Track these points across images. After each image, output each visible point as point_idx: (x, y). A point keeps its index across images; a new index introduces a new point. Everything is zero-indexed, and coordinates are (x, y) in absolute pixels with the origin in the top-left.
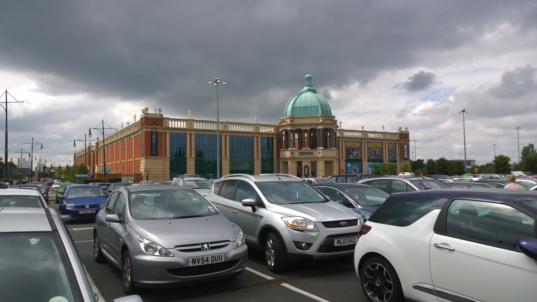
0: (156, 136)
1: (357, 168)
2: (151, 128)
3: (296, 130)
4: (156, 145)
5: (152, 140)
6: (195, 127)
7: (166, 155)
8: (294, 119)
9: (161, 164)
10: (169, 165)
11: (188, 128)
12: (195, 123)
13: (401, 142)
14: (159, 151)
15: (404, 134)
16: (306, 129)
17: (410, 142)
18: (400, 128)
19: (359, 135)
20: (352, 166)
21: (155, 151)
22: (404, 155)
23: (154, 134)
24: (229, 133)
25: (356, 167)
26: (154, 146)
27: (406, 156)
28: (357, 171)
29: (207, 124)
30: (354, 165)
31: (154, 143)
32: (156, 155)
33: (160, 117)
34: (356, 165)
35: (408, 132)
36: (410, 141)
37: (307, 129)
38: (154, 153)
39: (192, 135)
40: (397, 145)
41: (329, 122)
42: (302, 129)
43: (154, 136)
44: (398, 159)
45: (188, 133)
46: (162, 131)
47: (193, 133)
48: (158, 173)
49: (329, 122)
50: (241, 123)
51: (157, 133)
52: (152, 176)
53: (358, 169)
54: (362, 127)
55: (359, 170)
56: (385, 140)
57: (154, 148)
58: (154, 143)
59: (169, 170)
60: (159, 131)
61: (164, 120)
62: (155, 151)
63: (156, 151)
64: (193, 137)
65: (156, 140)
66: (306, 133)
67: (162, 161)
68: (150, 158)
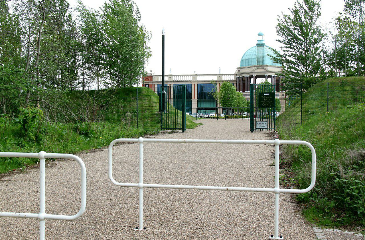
8: (242, 69)
24: (156, 83)
41: (264, 70)
45: (193, 83)
46: (152, 83)
47: (196, 83)
49: (264, 70)
60: (150, 84)
61: (153, 77)
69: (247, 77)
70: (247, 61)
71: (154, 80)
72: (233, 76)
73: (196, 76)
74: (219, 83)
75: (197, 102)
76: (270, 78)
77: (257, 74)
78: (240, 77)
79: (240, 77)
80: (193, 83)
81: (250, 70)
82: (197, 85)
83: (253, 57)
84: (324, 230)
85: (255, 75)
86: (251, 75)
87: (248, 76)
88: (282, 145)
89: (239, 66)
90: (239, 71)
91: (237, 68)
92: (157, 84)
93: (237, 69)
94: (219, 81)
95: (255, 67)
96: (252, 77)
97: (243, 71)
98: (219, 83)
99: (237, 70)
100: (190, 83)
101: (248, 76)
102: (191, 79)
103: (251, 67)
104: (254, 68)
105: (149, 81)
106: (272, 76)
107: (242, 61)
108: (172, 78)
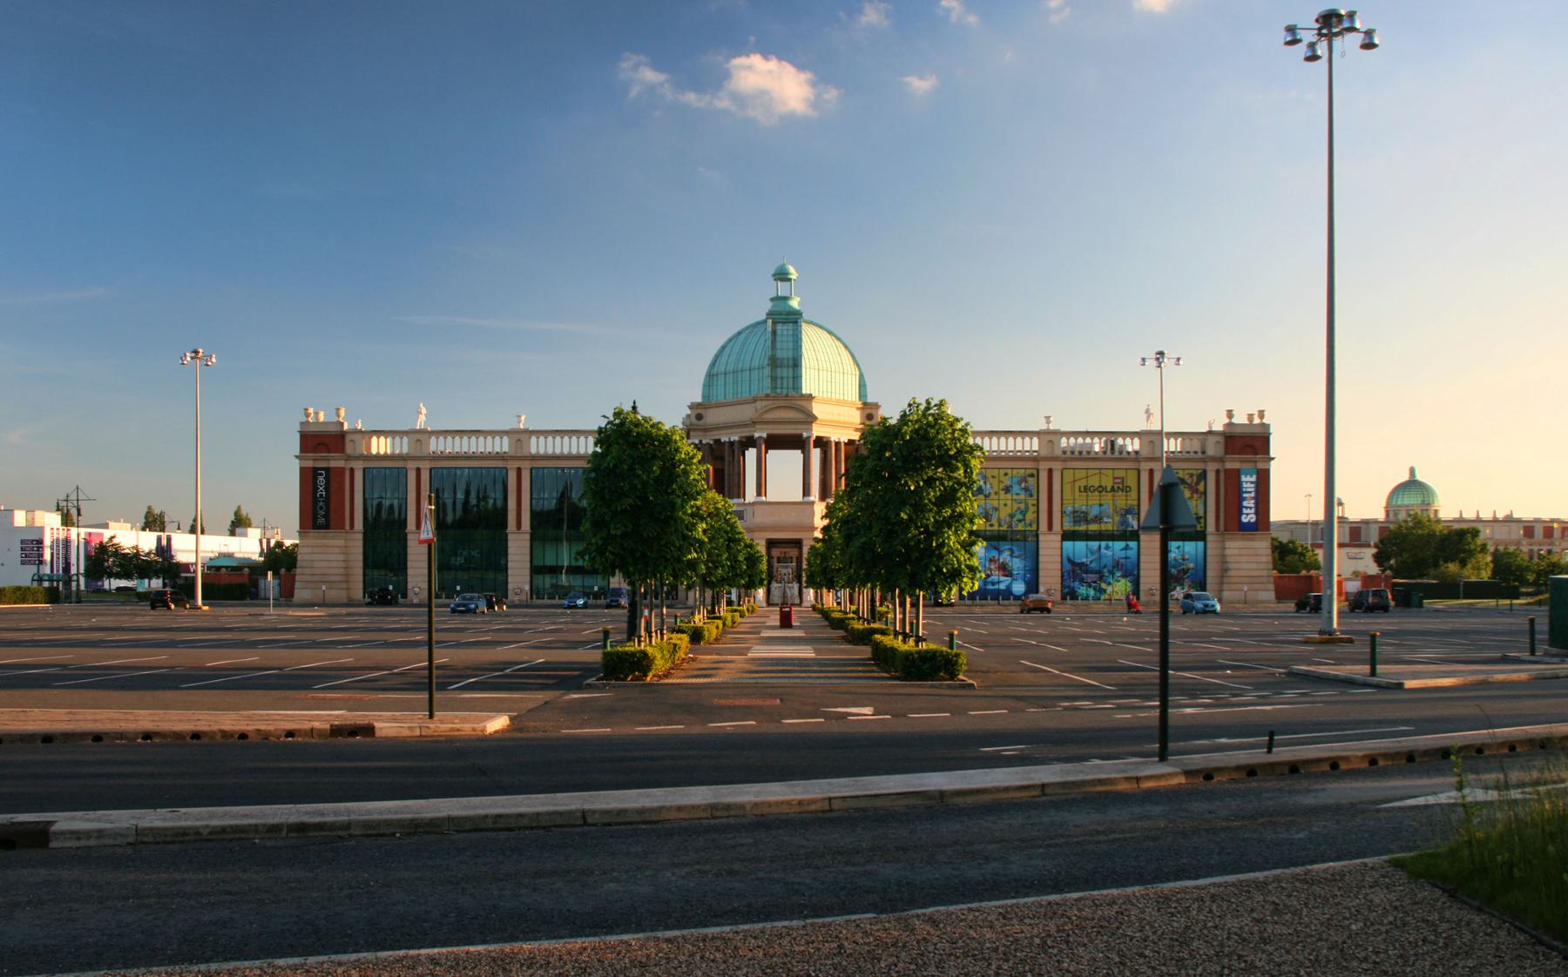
0: (327, 478)
1: (1016, 560)
2: (314, 460)
3: (712, 442)
4: (327, 500)
5: (315, 489)
6: (533, 451)
7: (352, 526)
8: (708, 410)
9: (337, 550)
10: (509, 556)
11: (413, 453)
12: (374, 439)
13: (1229, 465)
14: (332, 515)
15: (1242, 437)
16: (701, 441)
17: (1272, 462)
18: (1230, 414)
19: (1033, 445)
20: (994, 553)
21: (323, 516)
22: (1240, 513)
23: (322, 474)
24: (427, 462)
25: (1011, 556)
26: (321, 504)
27: (1249, 516)
28: (1015, 573)
29: (457, 438)
30: (1000, 552)
31: (321, 495)
32: (327, 526)
33: (337, 429)
34: (1011, 550)
35: (1267, 427)
36: (1273, 459)
37: (732, 440)
38: (321, 521)
39: (422, 471)
40: (1211, 477)
41: (791, 415)
42: (722, 441)
43: (321, 478)
44: (1211, 527)
45: (411, 465)
46: (341, 464)
47: (526, 466)
48: (331, 571)
49: (791, 415)
50: (561, 431)
51: (327, 470)
52: (306, 578)
53: (1017, 564)
54: (1046, 417)
55: (1021, 566)
56: (1051, 458)
57: (321, 508)
58: (321, 495)
59: (361, 564)
60: (333, 464)
61: (348, 438)
62: (323, 516)
63: (327, 516)
64: (425, 476)
65: (327, 489)
66: (1062, 446)
67: (341, 542)
68: (1258, 536)
69: (731, 444)
70: (730, 378)
71: (349, 449)
72: (506, 439)
73: (524, 437)
74: (516, 464)
75: (528, 544)
76: (750, 449)
77: (770, 432)
78: (704, 442)
79: (704, 442)
80: (411, 465)
81: (747, 412)
82: (529, 471)
83: (755, 363)
84: (1199, 502)
85: (765, 435)
86: (746, 432)
87: (735, 438)
88: (1231, 437)
89: (699, 399)
90: (699, 417)
91: (692, 407)
92: (429, 467)
93: (689, 412)
94: (1046, 459)
95: (765, 403)
96: (750, 442)
97: (712, 417)
98: (516, 464)
99: (688, 416)
100: (500, 464)
101: (737, 438)
102: (506, 449)
103: (745, 402)
104: (759, 404)
105: (329, 452)
106: (832, 439)
107: (711, 377)
108: (429, 444)
